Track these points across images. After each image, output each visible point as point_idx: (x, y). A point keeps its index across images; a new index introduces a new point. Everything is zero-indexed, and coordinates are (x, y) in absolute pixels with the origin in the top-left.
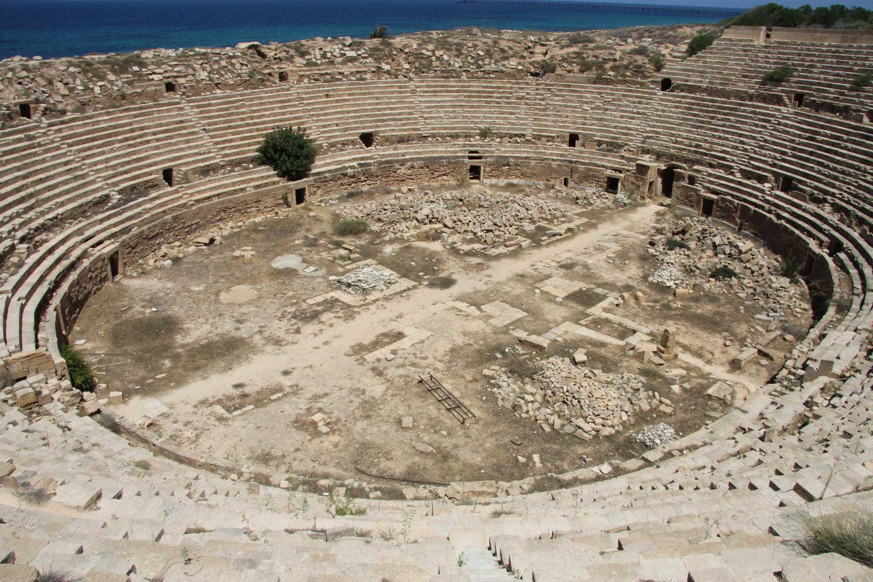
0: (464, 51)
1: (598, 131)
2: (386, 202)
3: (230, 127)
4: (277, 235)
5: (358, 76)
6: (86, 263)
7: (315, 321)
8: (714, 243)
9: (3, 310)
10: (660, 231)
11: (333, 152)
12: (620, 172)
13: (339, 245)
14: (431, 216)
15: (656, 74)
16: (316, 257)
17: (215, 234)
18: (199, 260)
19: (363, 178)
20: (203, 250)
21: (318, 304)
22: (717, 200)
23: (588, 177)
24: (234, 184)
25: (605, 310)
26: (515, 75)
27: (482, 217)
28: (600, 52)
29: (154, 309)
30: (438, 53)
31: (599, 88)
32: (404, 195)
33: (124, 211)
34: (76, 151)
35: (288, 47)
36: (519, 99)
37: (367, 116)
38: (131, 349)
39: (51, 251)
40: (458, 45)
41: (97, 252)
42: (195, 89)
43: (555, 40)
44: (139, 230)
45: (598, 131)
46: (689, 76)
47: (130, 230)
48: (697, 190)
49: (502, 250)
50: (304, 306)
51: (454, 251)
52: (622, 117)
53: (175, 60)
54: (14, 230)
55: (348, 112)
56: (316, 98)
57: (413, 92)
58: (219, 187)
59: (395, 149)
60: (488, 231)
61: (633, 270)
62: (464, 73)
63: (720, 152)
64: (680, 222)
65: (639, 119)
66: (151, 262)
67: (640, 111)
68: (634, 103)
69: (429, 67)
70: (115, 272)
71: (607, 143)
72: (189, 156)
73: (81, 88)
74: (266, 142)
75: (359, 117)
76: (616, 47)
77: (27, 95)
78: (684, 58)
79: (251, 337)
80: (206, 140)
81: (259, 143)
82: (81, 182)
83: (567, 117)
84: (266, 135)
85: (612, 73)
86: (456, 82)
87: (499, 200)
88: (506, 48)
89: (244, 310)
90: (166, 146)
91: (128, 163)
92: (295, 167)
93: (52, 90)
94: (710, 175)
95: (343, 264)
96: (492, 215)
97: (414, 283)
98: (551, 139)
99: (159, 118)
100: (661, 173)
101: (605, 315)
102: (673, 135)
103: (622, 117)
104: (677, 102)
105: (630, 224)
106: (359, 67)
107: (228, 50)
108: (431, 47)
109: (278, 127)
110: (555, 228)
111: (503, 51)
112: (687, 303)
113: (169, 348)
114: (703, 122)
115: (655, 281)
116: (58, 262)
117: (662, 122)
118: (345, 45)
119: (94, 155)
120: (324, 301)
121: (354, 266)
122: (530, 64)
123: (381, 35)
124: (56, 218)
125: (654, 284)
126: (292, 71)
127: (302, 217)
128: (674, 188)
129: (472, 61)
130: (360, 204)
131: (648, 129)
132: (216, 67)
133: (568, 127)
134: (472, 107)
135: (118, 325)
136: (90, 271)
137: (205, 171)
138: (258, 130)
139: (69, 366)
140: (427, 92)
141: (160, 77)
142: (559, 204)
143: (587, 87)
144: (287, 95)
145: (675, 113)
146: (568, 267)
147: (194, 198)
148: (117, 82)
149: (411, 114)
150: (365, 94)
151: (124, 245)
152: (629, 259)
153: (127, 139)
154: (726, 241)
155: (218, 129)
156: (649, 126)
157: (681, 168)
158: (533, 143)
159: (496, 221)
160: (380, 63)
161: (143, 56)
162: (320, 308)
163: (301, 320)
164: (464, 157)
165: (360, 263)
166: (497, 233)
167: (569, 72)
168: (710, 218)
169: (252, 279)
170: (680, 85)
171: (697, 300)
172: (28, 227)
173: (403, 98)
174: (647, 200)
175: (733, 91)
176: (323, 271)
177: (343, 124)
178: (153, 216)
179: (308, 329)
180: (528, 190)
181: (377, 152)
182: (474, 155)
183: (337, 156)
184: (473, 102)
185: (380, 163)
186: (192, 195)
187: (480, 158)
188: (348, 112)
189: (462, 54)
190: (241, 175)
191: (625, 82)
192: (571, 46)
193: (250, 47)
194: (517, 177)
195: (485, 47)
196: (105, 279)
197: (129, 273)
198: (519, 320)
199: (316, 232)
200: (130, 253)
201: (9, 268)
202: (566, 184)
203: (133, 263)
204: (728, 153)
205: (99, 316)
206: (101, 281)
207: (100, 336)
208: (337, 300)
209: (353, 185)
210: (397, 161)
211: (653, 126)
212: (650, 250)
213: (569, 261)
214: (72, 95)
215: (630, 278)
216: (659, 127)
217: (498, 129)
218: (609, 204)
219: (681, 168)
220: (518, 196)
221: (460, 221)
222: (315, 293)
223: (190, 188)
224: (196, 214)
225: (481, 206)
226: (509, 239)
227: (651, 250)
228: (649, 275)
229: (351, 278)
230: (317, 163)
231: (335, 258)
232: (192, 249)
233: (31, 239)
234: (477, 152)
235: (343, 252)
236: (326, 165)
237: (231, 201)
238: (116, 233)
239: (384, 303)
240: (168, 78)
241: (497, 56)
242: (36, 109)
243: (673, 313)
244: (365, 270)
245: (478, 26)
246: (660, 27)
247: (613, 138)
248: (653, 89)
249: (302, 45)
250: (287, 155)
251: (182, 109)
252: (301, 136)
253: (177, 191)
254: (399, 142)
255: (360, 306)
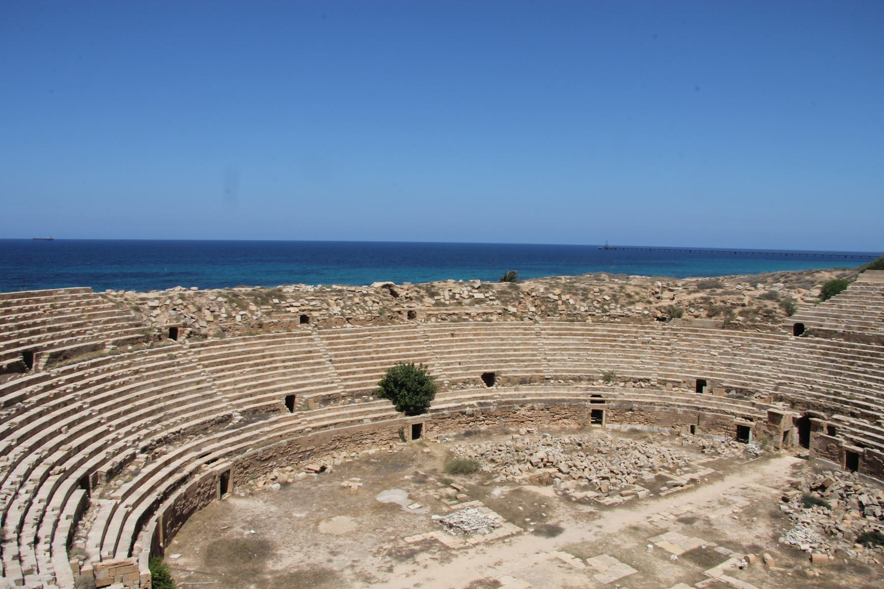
0: (590, 296)
1: (726, 376)
2: (502, 443)
3: (355, 360)
4: (388, 468)
5: (484, 317)
6: (197, 478)
7: (410, 561)
8: (860, 503)
9: (108, 515)
10: (795, 486)
11: (454, 389)
12: (751, 420)
13: (447, 483)
14: (545, 460)
15: (787, 319)
16: (423, 494)
17: (327, 463)
18: (307, 487)
19: (481, 418)
20: (313, 477)
21: (416, 543)
22: (863, 453)
23: (716, 424)
24: (352, 414)
25: (727, 572)
26: (641, 319)
27: (599, 463)
28: (728, 297)
29: (253, 532)
30: (564, 298)
31: (727, 333)
32: (520, 437)
33: (243, 431)
34: (209, 372)
35: (420, 287)
36: (645, 343)
37: (490, 356)
38: (222, 569)
39: (167, 463)
40: (585, 289)
41: (209, 469)
42: (327, 323)
43: (683, 285)
44: (254, 452)
45: (726, 376)
46: (824, 321)
47: (245, 451)
48: (838, 442)
49: (617, 499)
50: (402, 543)
51: (566, 497)
52: (752, 362)
53: (313, 295)
54: (139, 440)
55: (472, 352)
56: (441, 336)
57: (538, 334)
58: (338, 416)
59: (516, 390)
60: (604, 478)
61: (762, 529)
62: (589, 317)
63: (863, 400)
64: (820, 476)
65: (770, 364)
66: (261, 484)
67: (772, 356)
68: (764, 348)
69: (555, 310)
70: (224, 490)
71: (736, 389)
72: (312, 384)
73: (225, 315)
74: (388, 376)
75: (483, 356)
76: (745, 292)
77: (178, 319)
78: (817, 303)
79: (342, 571)
80: (331, 370)
81: (381, 376)
82: (209, 400)
83: (694, 362)
84: (389, 370)
85: (740, 318)
86: (581, 325)
87: (619, 446)
88: (633, 294)
89: (339, 542)
90: (292, 373)
91: (255, 386)
92: (413, 402)
93: (200, 316)
94: (852, 425)
95: (449, 503)
96: (610, 462)
97: (518, 529)
98: (677, 384)
99: (290, 347)
100: (796, 422)
101: (725, 578)
102: (808, 382)
103: (752, 362)
104: (811, 347)
105: (762, 476)
106: (485, 309)
107: (364, 289)
108: (557, 291)
109: (400, 363)
110: (677, 478)
111: (629, 296)
112: (827, 572)
113: (258, 573)
114: (841, 368)
115: (787, 543)
116: (171, 474)
117: (796, 368)
118: (473, 288)
119: (224, 377)
120: (422, 541)
121: (459, 506)
122: (657, 309)
123: (511, 279)
124: (179, 432)
125: (786, 545)
126: (421, 310)
127: (415, 453)
128: (812, 439)
129: (598, 306)
130: (476, 443)
131: (780, 375)
132: (349, 303)
133: (694, 372)
134: (597, 350)
135: (214, 543)
136: (199, 486)
137: (326, 400)
138: (382, 364)
139: (153, 579)
140: (552, 335)
141: (297, 309)
142: (684, 453)
143: (715, 332)
144: (413, 332)
145: (809, 358)
146: (688, 521)
147: (312, 425)
148: (256, 312)
149: (535, 355)
150: (489, 335)
151: (236, 464)
152: (757, 515)
153: (257, 365)
154: (875, 501)
155: (344, 361)
156: (782, 372)
157: (819, 417)
158: (658, 388)
159: (614, 468)
160: (507, 305)
161: (284, 290)
162: (417, 548)
163: (396, 558)
164: (586, 401)
165: (466, 504)
166: (613, 480)
167: (696, 317)
168: (856, 473)
169: (354, 511)
170: (814, 330)
171: (840, 568)
172: (151, 438)
173: (527, 340)
174: (783, 451)
175: (873, 336)
176: (428, 509)
177: (466, 363)
178: (269, 439)
179: (402, 568)
180: (651, 437)
181: (497, 392)
182: (596, 399)
183: (457, 394)
184: (597, 345)
185: (500, 403)
186: (310, 422)
187: (603, 402)
188: (472, 352)
189: (588, 299)
190: (360, 406)
191: (754, 327)
192: (698, 292)
193: (384, 286)
194: (640, 423)
195: (611, 292)
196: (213, 496)
197: (237, 493)
198: (626, 577)
199: (427, 468)
200: (241, 473)
201: (125, 475)
202: (693, 431)
203: (243, 483)
204: (872, 401)
205: (199, 532)
206: (208, 498)
207: (195, 553)
208: (436, 541)
209: (471, 424)
210: (517, 402)
211: (786, 373)
212: (782, 507)
213: (689, 515)
214: (216, 321)
215: (757, 537)
216: (793, 373)
217: (622, 373)
218: (738, 454)
219: (819, 417)
220: (640, 443)
221: (575, 466)
222: (416, 531)
223: (310, 415)
224: (311, 441)
225: (599, 452)
226: (626, 488)
227: (784, 507)
228: (780, 535)
229: (453, 519)
230: (437, 399)
231: (441, 497)
232: (302, 474)
233: (152, 450)
234: (599, 396)
235: (450, 491)
236: (445, 402)
237: (346, 431)
238: (231, 452)
239: (484, 548)
240: (304, 311)
241: (623, 301)
242: (183, 332)
243: (809, 582)
244: (469, 511)
245: (606, 271)
246: (796, 272)
247: (743, 384)
248: (785, 334)
249: (433, 286)
250: (408, 390)
251: (312, 340)
252: (422, 373)
253: (296, 417)
254: (521, 383)
255: (459, 549)
